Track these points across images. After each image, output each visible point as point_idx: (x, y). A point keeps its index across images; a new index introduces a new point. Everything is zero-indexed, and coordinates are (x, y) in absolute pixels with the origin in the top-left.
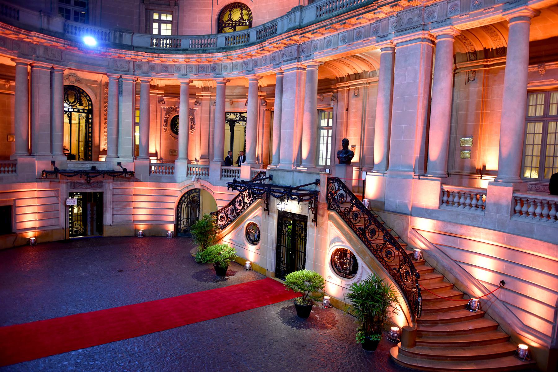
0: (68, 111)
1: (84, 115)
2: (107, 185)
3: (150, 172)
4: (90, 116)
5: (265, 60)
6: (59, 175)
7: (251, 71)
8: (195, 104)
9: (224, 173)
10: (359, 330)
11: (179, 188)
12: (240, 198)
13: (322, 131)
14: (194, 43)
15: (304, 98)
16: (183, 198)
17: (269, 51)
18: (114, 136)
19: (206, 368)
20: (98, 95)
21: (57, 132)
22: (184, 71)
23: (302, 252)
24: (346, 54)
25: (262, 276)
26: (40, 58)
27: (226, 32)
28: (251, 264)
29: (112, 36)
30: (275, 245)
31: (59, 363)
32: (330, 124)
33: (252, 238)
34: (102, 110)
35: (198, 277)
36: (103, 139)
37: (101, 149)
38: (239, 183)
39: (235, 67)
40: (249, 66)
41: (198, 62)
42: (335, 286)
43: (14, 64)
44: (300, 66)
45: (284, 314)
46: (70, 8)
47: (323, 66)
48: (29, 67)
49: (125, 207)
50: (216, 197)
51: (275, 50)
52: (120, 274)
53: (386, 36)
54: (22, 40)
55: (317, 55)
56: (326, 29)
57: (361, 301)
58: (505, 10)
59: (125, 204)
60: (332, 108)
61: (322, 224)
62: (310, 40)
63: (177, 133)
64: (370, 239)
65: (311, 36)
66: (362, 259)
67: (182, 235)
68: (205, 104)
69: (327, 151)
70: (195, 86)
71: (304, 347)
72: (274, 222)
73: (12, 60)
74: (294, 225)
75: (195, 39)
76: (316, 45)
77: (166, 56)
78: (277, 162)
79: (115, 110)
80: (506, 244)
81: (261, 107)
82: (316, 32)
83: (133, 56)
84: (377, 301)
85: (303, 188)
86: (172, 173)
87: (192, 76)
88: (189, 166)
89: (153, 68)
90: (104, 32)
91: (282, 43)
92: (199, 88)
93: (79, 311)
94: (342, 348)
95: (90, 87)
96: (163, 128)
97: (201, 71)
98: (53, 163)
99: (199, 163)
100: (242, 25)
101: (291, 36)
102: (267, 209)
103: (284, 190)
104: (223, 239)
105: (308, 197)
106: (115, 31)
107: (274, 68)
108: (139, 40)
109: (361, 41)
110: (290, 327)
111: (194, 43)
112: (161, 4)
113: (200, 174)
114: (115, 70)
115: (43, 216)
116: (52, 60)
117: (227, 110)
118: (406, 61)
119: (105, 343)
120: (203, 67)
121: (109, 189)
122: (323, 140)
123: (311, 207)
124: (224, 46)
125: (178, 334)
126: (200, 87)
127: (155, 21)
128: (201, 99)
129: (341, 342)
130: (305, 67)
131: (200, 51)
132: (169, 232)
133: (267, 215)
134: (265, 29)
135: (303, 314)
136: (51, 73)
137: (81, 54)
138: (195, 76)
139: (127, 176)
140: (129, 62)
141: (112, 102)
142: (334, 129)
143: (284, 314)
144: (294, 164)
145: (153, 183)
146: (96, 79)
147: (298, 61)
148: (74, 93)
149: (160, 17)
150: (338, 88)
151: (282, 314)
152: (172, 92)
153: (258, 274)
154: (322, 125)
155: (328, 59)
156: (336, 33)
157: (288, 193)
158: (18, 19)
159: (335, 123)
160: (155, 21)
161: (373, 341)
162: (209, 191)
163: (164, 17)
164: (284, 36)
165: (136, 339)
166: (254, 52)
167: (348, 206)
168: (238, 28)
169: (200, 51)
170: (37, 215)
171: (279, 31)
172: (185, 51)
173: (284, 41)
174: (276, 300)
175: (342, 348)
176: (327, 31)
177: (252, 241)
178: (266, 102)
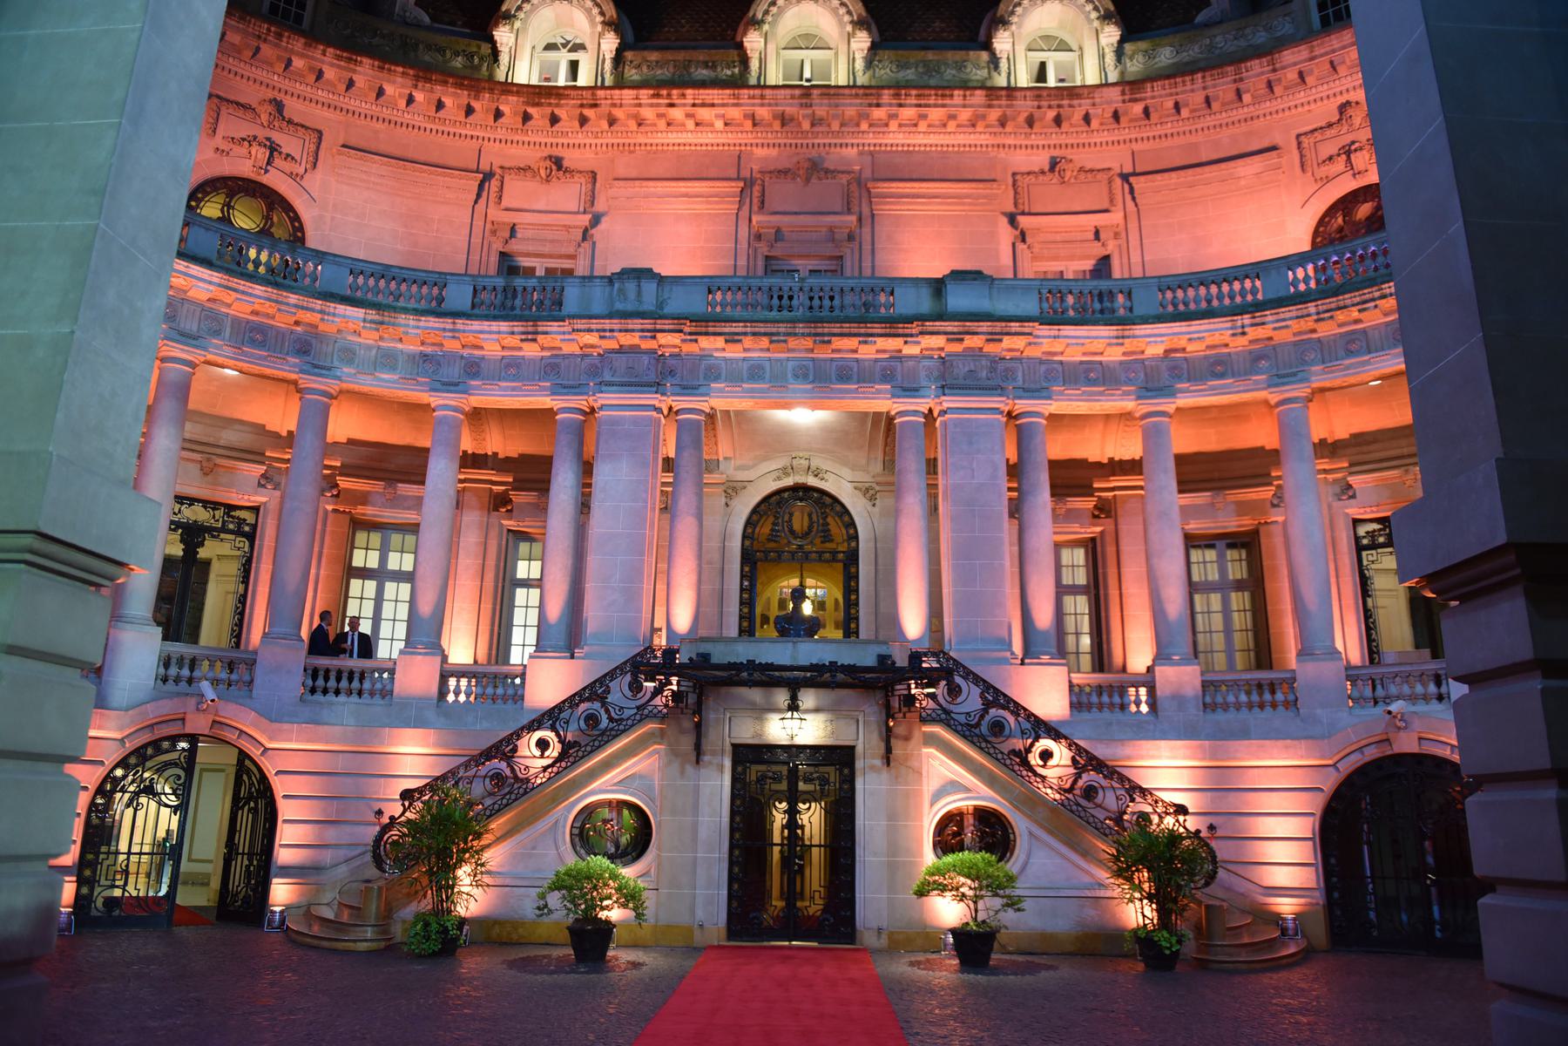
11: (121, 729)
53: (916, 390)
55: (721, 391)
58: (1139, 398)
61: (907, 758)
72: (718, 784)
80: (1211, 759)
118: (970, 443)
138: (228, 351)
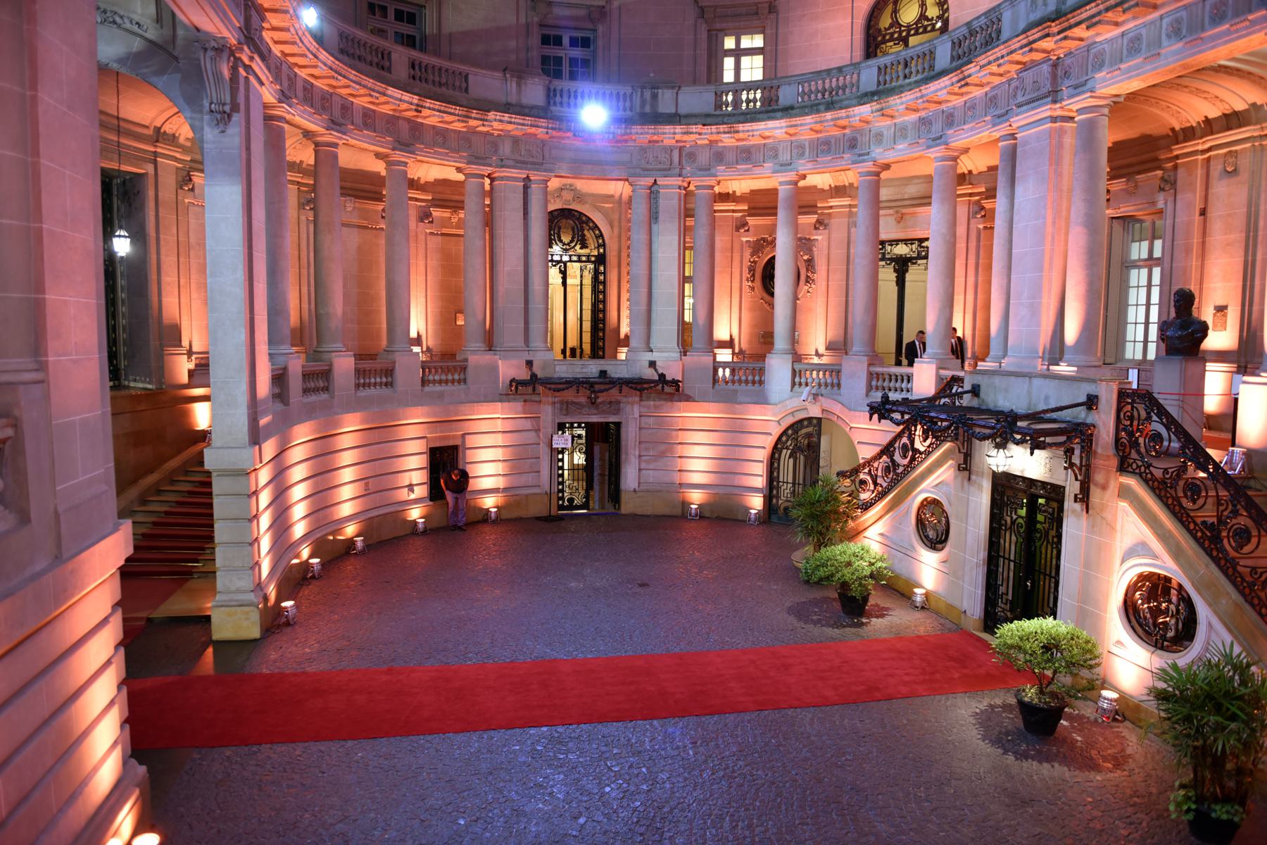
0: (560, 261)
1: (591, 266)
2: (628, 408)
3: (715, 380)
4: (602, 268)
5: (973, 107)
6: (540, 389)
7: (938, 140)
8: (816, 228)
9: (874, 383)
10: (1182, 786)
11: (774, 415)
12: (905, 440)
13: (1134, 273)
14: (813, 89)
15: (1070, 191)
16: (784, 439)
17: (982, 85)
18: (643, 307)
19: (783, 807)
20: (616, 224)
21: (536, 304)
22: (784, 157)
23: (1045, 575)
24: (1184, 67)
25: (949, 625)
26: (505, 162)
27: (885, 54)
28: (927, 595)
29: (637, 101)
30: (983, 555)
31: (504, 746)
32: (1157, 253)
33: (931, 534)
34: (624, 255)
35: (800, 612)
36: (625, 313)
37: (622, 336)
38: (895, 403)
39: (901, 132)
40: (935, 127)
41: (817, 132)
42: (1130, 666)
43: (461, 177)
44: (1059, 113)
45: (989, 719)
46: (561, 53)
47: (1121, 107)
48: (487, 181)
49: (662, 455)
50: (856, 437)
51: (997, 80)
52: (640, 590)
54: (473, 131)
55: (1104, 80)
56: (1124, 12)
57: (1185, 711)
59: (662, 447)
60: (1161, 212)
61: (1103, 508)
62: (1083, 44)
63: (772, 295)
64: (1232, 553)
65: (1085, 34)
66: (1210, 605)
67: (779, 518)
68: (838, 226)
69: (1147, 323)
70: (815, 187)
71: (1025, 803)
72: (982, 499)
73: (459, 170)
74: (1033, 508)
75: (809, 82)
76: (1102, 53)
77: (747, 126)
78: (1001, 353)
79: (644, 254)
81: (972, 221)
82: (1099, 22)
83: (678, 137)
84: (1233, 718)
85: (1054, 415)
86: (761, 382)
87: (803, 165)
88: (797, 367)
89: (719, 157)
90: (622, 93)
91: (1011, 62)
92: (823, 190)
93: (555, 655)
94: (1131, 824)
95: (599, 209)
96: (747, 284)
97: (822, 151)
98: (529, 364)
99: (825, 360)
100: (925, 31)
101: (1034, 41)
102: (966, 466)
103: (998, 421)
104: (867, 534)
105: (1062, 439)
106: (643, 88)
107: (994, 125)
108: (694, 99)
109: (1225, 27)
110: (1000, 751)
111: (813, 89)
112: (740, 15)
113: (820, 385)
114: (644, 170)
115: (512, 468)
116: (524, 163)
117: (883, 237)
119: (590, 722)
120: (827, 142)
121: (633, 418)
122: (1136, 296)
123: (1071, 465)
124: (873, 88)
125: (736, 727)
126: (827, 188)
127: (729, 53)
128: (829, 214)
129: (1130, 810)
130: (1072, 114)
131: (822, 107)
132: (753, 512)
133: (966, 482)
134: (972, 33)
135: (1040, 724)
136: (526, 188)
137: (578, 144)
138: (810, 165)
139: (668, 389)
140: (671, 149)
141: (639, 236)
142: (1167, 265)
143: (989, 719)
144: (1043, 358)
145: (721, 406)
146: (611, 193)
147: (1055, 102)
148: (568, 223)
149: (738, 42)
150: (1177, 157)
151: (985, 720)
152: (763, 204)
153: (942, 621)
154: (1134, 256)
155: (1135, 85)
156: (1156, 15)
157: (1007, 428)
158: (466, 90)
159: (1170, 249)
160: (729, 53)
161: (1218, 820)
162: (840, 422)
163: (746, 42)
164: (1015, 44)
165: (651, 725)
166: (945, 91)
167: (1171, 464)
168: (913, 41)
169: (822, 107)
170: (500, 464)
171: (1005, 34)
172: (788, 111)
173: (1016, 57)
174: (977, 681)
175: (1131, 824)
176: (1128, 15)
177: (930, 541)
178: (983, 208)
